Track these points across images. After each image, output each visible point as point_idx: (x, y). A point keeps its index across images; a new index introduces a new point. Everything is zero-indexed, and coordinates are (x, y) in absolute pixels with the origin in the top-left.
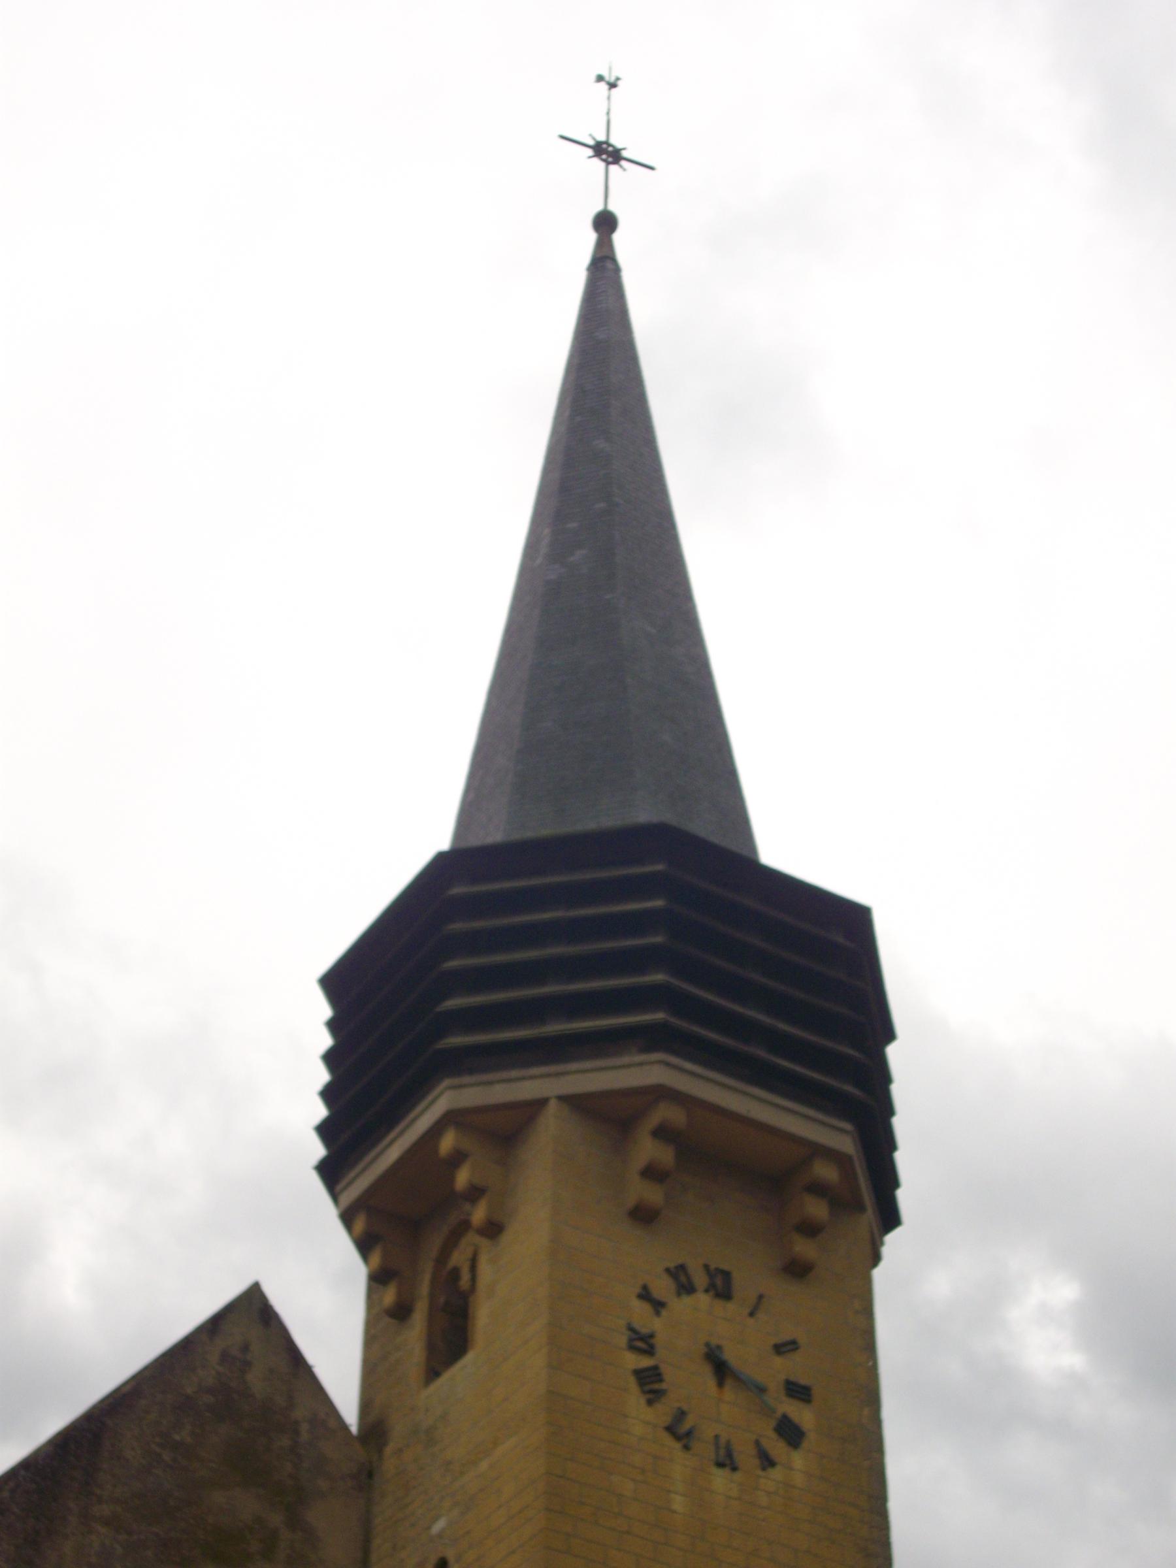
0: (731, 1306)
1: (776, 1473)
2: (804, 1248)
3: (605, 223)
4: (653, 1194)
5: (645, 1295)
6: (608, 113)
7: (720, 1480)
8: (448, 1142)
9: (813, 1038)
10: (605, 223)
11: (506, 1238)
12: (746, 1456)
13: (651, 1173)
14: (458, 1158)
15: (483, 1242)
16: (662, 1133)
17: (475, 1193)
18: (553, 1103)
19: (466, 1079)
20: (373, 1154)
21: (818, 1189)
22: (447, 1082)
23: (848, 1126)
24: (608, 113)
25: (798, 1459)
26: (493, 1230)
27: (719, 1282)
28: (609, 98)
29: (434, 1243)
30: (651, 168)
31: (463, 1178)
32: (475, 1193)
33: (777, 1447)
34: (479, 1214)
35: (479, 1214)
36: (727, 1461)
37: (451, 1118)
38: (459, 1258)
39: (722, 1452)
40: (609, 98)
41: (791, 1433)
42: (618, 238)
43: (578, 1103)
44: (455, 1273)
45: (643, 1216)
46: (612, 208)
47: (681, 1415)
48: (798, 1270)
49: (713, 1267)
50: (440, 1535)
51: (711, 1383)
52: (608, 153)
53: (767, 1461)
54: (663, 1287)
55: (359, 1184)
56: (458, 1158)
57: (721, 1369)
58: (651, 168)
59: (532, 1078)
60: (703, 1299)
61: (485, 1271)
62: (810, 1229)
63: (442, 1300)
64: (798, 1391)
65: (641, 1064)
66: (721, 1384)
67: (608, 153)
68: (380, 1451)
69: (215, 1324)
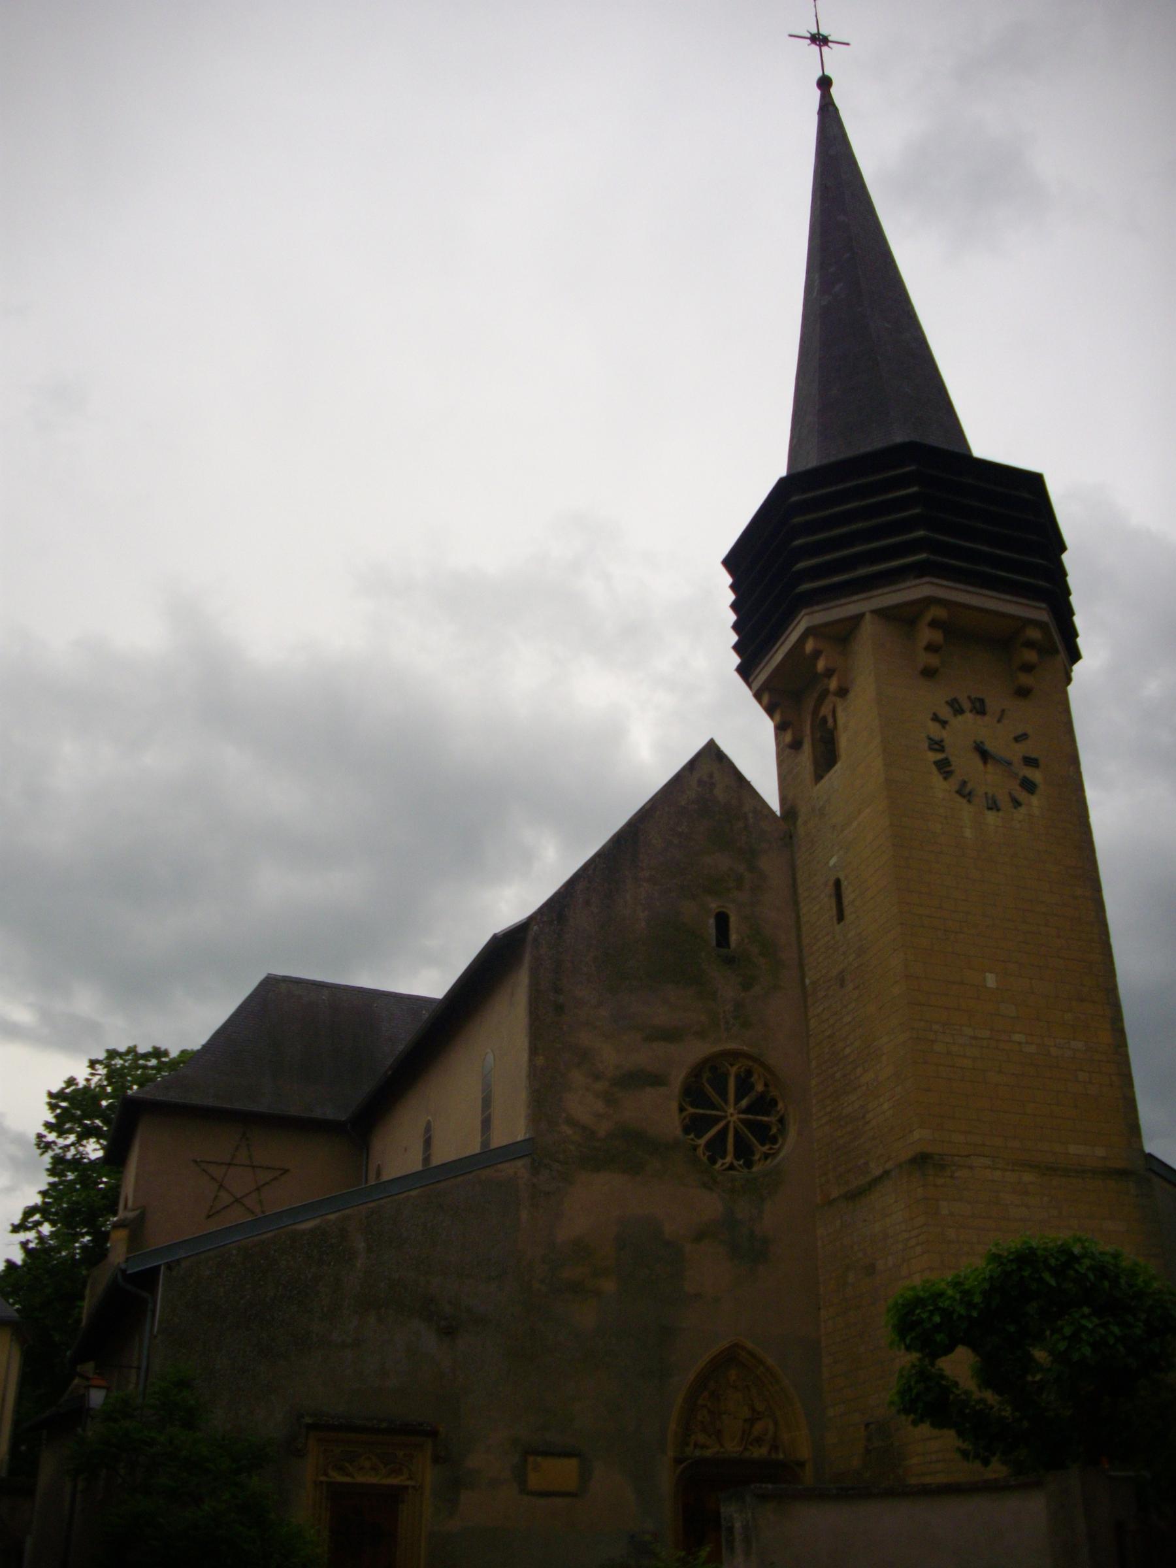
0: (987, 718)
1: (1023, 810)
2: (1025, 679)
3: (825, 83)
4: (934, 660)
5: (935, 718)
7: (991, 817)
8: (810, 646)
10: (825, 83)
11: (851, 695)
12: (1004, 801)
13: (931, 648)
14: (817, 654)
16: (934, 624)
17: (829, 673)
18: (868, 617)
21: (1030, 644)
23: (1044, 605)
25: (1035, 800)
26: (843, 692)
27: (978, 705)
31: (821, 665)
32: (829, 673)
33: (1022, 795)
34: (833, 684)
35: (833, 684)
36: (994, 806)
37: (809, 632)
38: (825, 710)
39: (990, 802)
41: (1029, 786)
42: (833, 91)
43: (883, 614)
45: (929, 673)
46: (826, 73)
47: (964, 783)
48: (1023, 693)
51: (980, 764)
52: (820, 40)
53: (1017, 803)
54: (945, 712)
56: (817, 654)
57: (984, 754)
60: (969, 716)
62: (1028, 668)
64: (1030, 762)
65: (915, 586)
66: (985, 762)
67: (820, 40)
69: (692, 765)
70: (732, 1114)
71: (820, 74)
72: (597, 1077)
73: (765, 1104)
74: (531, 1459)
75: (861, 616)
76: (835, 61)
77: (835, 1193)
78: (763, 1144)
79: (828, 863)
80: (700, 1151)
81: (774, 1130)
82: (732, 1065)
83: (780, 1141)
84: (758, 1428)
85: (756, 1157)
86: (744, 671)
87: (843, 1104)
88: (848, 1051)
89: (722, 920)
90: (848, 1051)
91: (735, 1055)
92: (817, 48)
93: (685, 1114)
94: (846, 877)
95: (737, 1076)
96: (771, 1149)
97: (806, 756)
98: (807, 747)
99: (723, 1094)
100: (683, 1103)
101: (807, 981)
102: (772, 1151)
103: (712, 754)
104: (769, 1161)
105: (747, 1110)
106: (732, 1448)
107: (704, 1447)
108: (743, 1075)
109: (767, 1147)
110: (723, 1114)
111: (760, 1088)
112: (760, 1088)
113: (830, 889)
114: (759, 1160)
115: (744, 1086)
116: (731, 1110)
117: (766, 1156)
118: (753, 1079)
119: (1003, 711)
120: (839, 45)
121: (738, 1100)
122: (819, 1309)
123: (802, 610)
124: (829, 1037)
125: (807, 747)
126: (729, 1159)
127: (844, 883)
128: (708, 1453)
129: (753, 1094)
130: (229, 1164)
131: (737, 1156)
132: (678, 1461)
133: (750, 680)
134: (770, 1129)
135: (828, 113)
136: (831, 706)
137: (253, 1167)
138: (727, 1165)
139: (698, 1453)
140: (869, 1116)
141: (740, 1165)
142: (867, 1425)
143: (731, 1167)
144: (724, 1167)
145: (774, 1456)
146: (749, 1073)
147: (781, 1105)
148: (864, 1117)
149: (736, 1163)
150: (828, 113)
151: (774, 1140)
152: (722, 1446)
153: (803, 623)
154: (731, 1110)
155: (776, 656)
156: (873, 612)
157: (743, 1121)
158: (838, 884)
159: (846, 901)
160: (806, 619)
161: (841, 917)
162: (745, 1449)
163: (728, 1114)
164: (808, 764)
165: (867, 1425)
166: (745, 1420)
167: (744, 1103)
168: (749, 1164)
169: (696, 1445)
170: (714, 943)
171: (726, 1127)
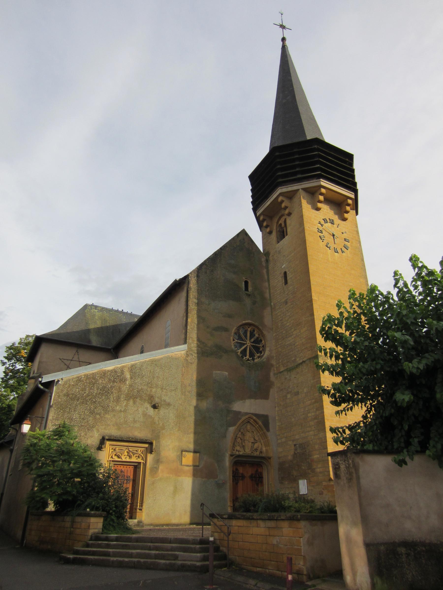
3: (283, 39)
5: (320, 223)
6: (282, 19)
8: (280, 199)
9: (350, 173)
10: (283, 39)
11: (292, 216)
12: (340, 251)
14: (282, 201)
15: (287, 217)
17: (286, 208)
18: (300, 189)
19: (283, 187)
20: (264, 204)
22: (280, 188)
24: (282, 19)
26: (289, 214)
27: (331, 221)
28: (282, 17)
29: (276, 220)
30: (274, 24)
31: (283, 205)
32: (286, 208)
33: (344, 249)
34: (287, 212)
35: (287, 212)
37: (280, 194)
38: (282, 221)
40: (282, 17)
44: (281, 224)
46: (284, 36)
49: (330, 219)
50: (284, 268)
52: (283, 27)
53: (343, 252)
54: (323, 222)
55: (260, 211)
56: (282, 201)
58: (274, 24)
59: (260, 210)
61: (288, 222)
63: (278, 229)
65: (317, 181)
67: (283, 27)
68: (269, 257)
69: (238, 235)
70: (248, 343)
71: (283, 37)
72: (208, 327)
73: (258, 341)
74: (184, 453)
75: (298, 190)
76: (287, 34)
77: (282, 369)
78: (258, 353)
79: (282, 267)
80: (239, 353)
81: (261, 349)
82: (249, 328)
83: (263, 353)
84: (256, 446)
85: (256, 357)
86: (255, 210)
87: (286, 341)
88: (288, 324)
89: (246, 283)
90: (288, 324)
91: (249, 325)
92: (283, 24)
93: (234, 341)
94: (289, 271)
95: (250, 331)
96: (260, 355)
97: (274, 236)
98: (274, 233)
99: (246, 336)
100: (234, 339)
101: (272, 304)
102: (260, 356)
103: (243, 235)
104: (259, 359)
105: (253, 342)
106: (248, 451)
107: (239, 451)
108: (252, 331)
109: (259, 354)
110: (246, 343)
111: (257, 335)
112: (257, 335)
113: (282, 274)
114: (257, 358)
115: (252, 335)
116: (248, 342)
117: (259, 357)
118: (255, 333)
119: (339, 224)
120: (289, 28)
121: (250, 339)
122: (275, 407)
123: (278, 187)
124: (281, 320)
125: (274, 233)
126: (248, 357)
127: (288, 273)
128: (241, 453)
129: (255, 337)
130: (71, 360)
131: (250, 357)
132: (231, 455)
133: (257, 212)
134: (260, 349)
135: (284, 48)
136: (284, 220)
137: (79, 361)
138: (247, 359)
139: (237, 453)
140: (296, 344)
141: (251, 359)
142: (295, 445)
143: (248, 360)
144: (246, 360)
145: (261, 455)
146: (254, 331)
147: (263, 342)
148: (294, 344)
149: (250, 359)
150: (284, 48)
151: (261, 353)
152: (245, 451)
153: (280, 190)
154: (248, 342)
155: (267, 204)
156: (302, 189)
157: (252, 346)
158: (285, 273)
159: (288, 278)
160: (280, 190)
161: (286, 283)
162: (252, 452)
163: (248, 343)
164: (275, 238)
165: (295, 445)
166: (252, 443)
167: (252, 340)
168: (253, 359)
169: (237, 450)
170: (244, 290)
171: (247, 347)
